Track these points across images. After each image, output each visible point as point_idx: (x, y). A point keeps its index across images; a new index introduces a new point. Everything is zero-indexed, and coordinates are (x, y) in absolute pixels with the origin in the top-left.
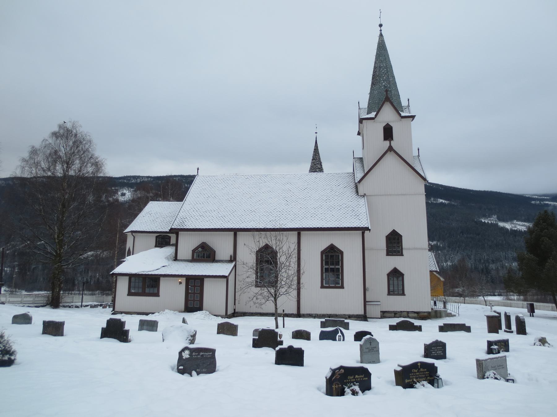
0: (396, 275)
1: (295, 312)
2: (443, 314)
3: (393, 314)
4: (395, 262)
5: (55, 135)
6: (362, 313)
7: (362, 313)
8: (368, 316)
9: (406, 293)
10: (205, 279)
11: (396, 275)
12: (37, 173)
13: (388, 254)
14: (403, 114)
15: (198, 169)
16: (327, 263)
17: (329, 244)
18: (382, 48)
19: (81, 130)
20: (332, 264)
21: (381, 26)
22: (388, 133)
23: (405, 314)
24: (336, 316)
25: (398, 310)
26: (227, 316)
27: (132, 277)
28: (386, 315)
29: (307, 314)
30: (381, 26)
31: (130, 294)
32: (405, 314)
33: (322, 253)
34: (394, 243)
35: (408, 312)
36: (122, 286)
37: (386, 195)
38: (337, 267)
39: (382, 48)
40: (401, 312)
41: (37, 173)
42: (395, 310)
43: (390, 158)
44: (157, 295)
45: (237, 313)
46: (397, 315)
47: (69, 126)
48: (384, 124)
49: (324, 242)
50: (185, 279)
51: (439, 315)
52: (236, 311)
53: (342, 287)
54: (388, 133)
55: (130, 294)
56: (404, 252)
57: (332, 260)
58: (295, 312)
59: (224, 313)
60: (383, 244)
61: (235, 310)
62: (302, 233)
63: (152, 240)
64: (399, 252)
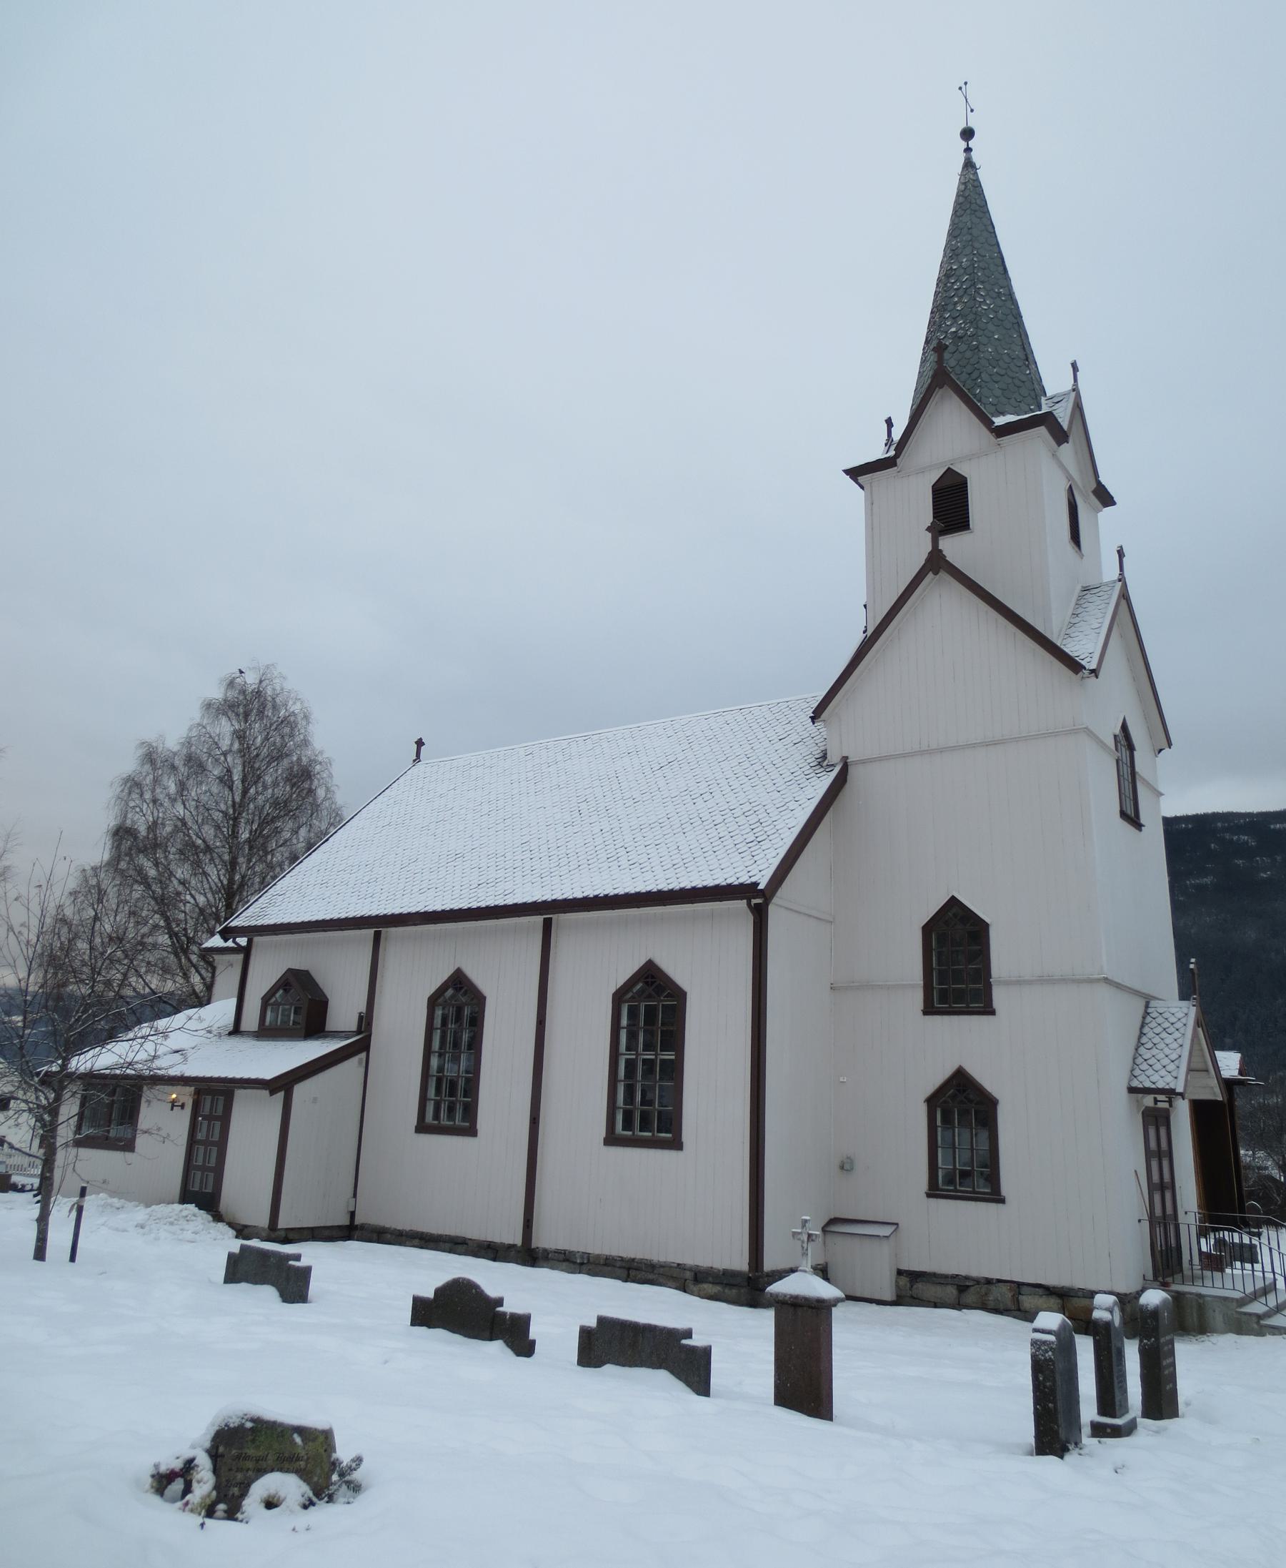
0: (962, 1109)
1: (514, 1236)
2: (1217, 1319)
3: (951, 1291)
4: (959, 1043)
6: (738, 1261)
7: (738, 1261)
8: (347, 1223)
9: (1006, 1187)
10: (240, 1094)
11: (962, 1109)
13: (929, 1010)
14: (999, 421)
15: (420, 743)
18: (971, 208)
19: (288, 686)
21: (968, 134)
22: (951, 506)
23: (1004, 1294)
25: (975, 1273)
26: (274, 1233)
28: (922, 1289)
29: (557, 1252)
30: (968, 134)
32: (1004, 1294)
34: (957, 960)
35: (1020, 1285)
37: (922, 753)
39: (971, 208)
40: (989, 1282)
42: (963, 1272)
44: (129, 1146)
45: (363, 1227)
46: (970, 1297)
48: (935, 476)
50: (190, 1089)
51: (1192, 1318)
52: (358, 1221)
53: (676, 1144)
54: (951, 506)
58: (514, 1236)
59: (263, 1221)
61: (353, 1214)
62: (560, 919)
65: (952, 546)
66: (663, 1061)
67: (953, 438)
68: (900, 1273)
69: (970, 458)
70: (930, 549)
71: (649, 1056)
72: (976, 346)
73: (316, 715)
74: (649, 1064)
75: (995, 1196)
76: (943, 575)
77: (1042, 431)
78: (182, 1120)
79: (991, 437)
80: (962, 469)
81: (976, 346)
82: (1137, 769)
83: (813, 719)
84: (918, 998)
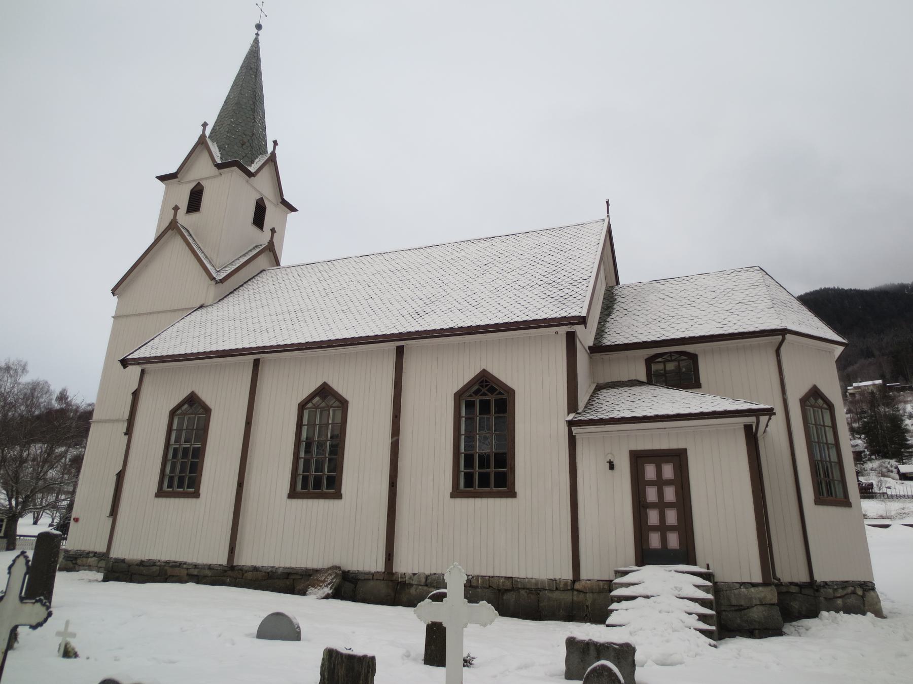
18: (251, 68)
21: (259, 27)
22: (195, 201)
30: (259, 27)
39: (251, 68)
45: (242, 570)
53: (293, 494)
54: (195, 201)
66: (194, 448)
69: (206, 178)
70: (172, 218)
71: (187, 446)
72: (240, 135)
74: (186, 451)
76: (271, 254)
79: (215, 169)
81: (240, 135)
82: (151, 240)
83: (114, 291)
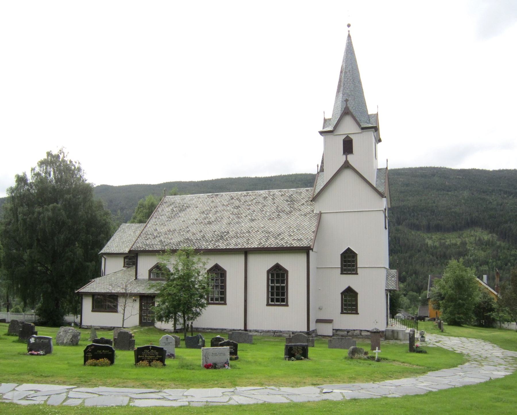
4: (349, 281)
5: (42, 163)
12: (507, 289)
16: (272, 282)
17: (275, 263)
18: (350, 51)
20: (278, 282)
21: (349, 26)
22: (348, 146)
24: (281, 332)
25: (351, 329)
27: (93, 295)
30: (349, 26)
31: (93, 310)
33: (268, 272)
34: (349, 261)
35: (361, 330)
36: (87, 304)
38: (278, 285)
39: (350, 51)
40: (354, 330)
41: (507, 289)
43: (348, 174)
47: (55, 152)
48: (344, 137)
49: (269, 261)
54: (348, 146)
55: (93, 310)
56: (359, 271)
57: (278, 279)
60: (338, 263)
63: (280, 350)
64: (353, 270)
65: (350, 157)
67: (349, 127)
68: (333, 330)
71: (278, 285)
73: (83, 167)
74: (278, 288)
75: (357, 313)
77: (373, 129)
78: (137, 305)
80: (351, 136)
84: (339, 271)
